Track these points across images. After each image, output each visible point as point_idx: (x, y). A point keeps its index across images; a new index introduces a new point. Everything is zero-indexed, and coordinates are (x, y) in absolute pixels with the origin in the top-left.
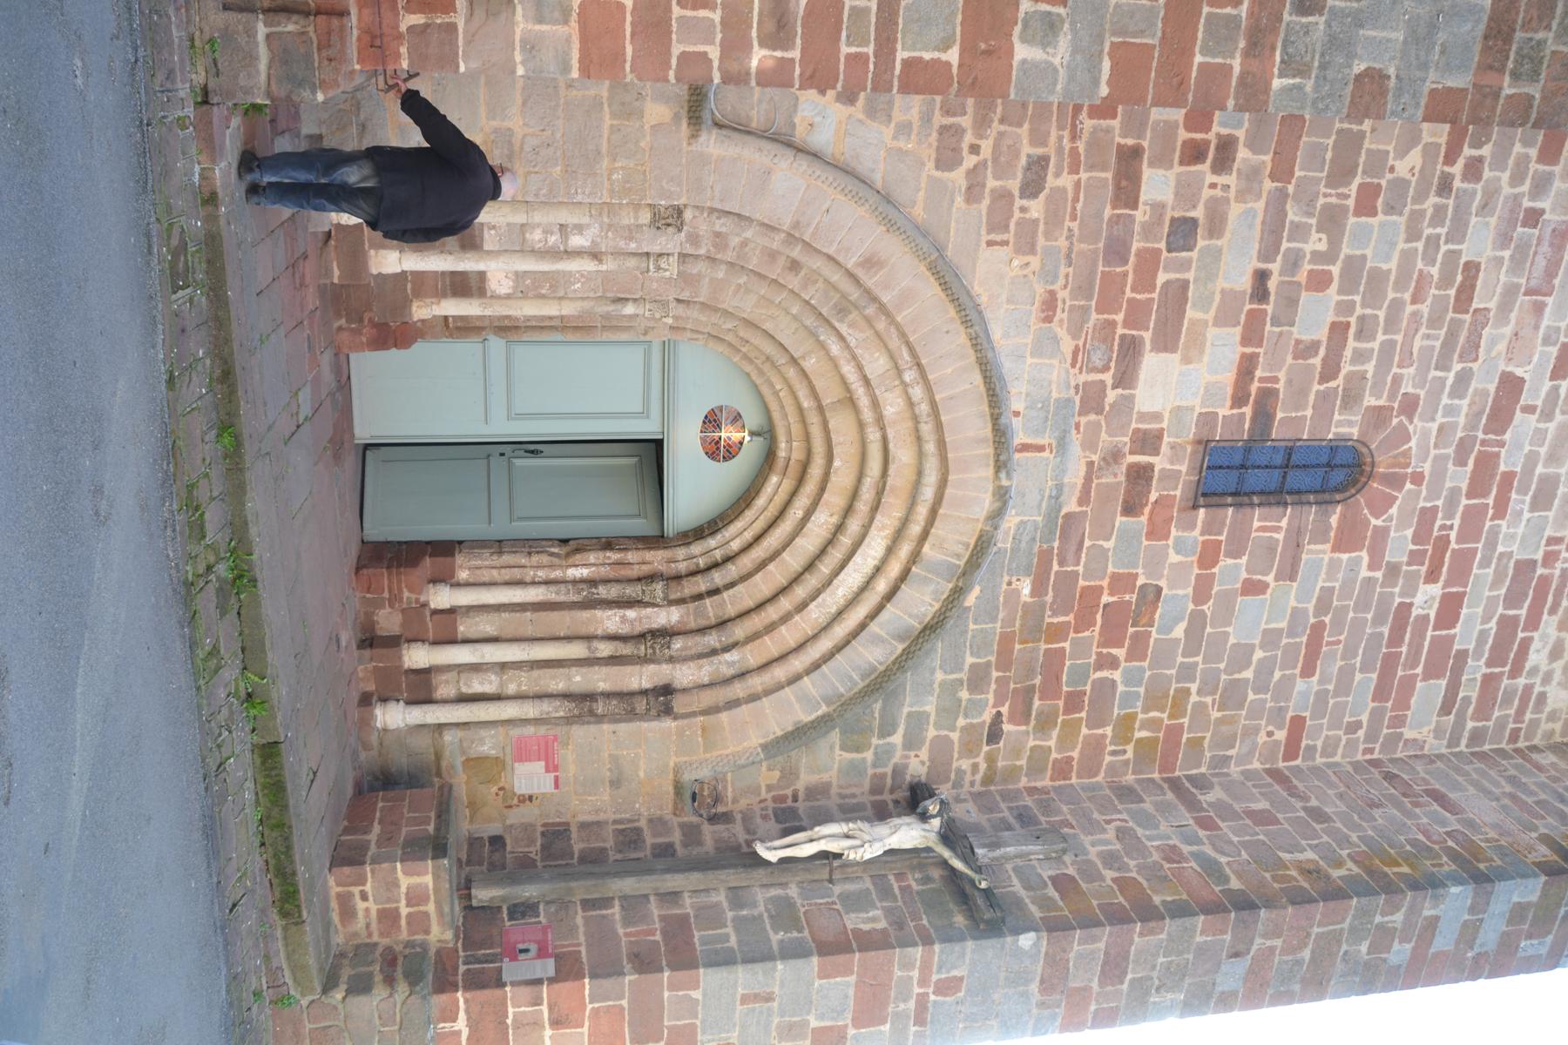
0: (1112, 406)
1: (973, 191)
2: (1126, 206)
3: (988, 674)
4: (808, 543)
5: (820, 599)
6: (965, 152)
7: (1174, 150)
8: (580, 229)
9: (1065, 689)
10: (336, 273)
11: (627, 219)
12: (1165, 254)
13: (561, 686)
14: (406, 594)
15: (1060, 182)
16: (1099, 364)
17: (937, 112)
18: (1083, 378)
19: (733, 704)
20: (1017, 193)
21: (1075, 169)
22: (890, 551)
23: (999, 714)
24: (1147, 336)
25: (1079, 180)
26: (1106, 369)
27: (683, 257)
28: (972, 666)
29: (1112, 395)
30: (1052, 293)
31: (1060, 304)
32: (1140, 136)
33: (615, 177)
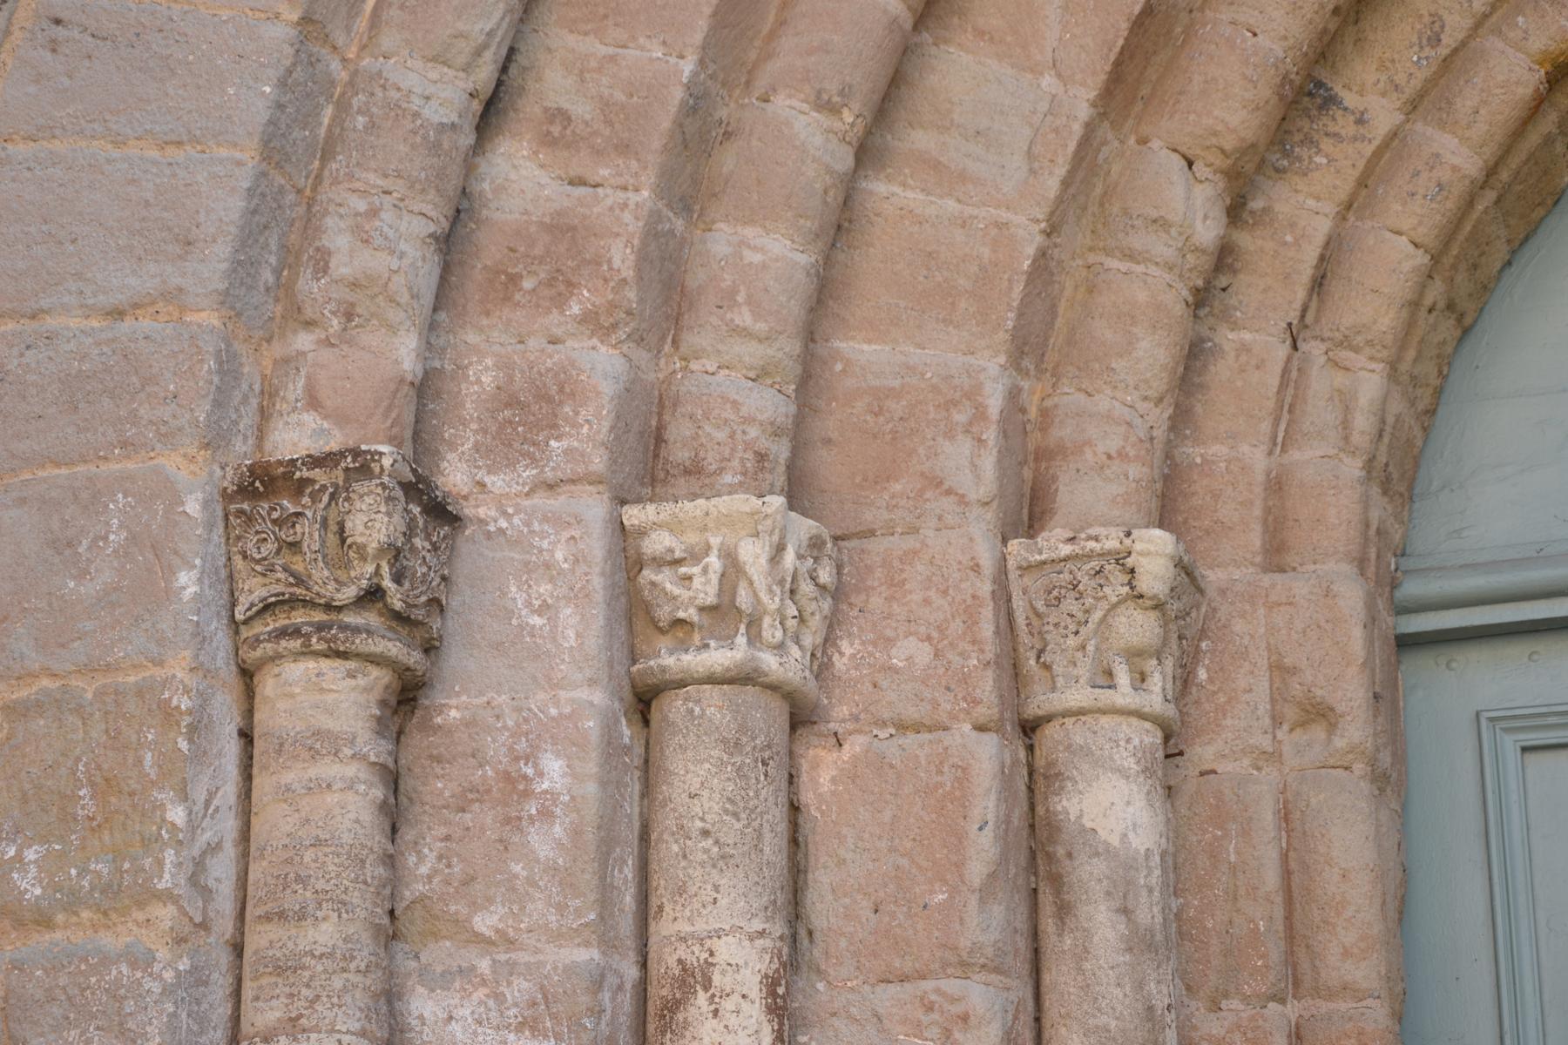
11: (327, 798)
27: (650, 459)
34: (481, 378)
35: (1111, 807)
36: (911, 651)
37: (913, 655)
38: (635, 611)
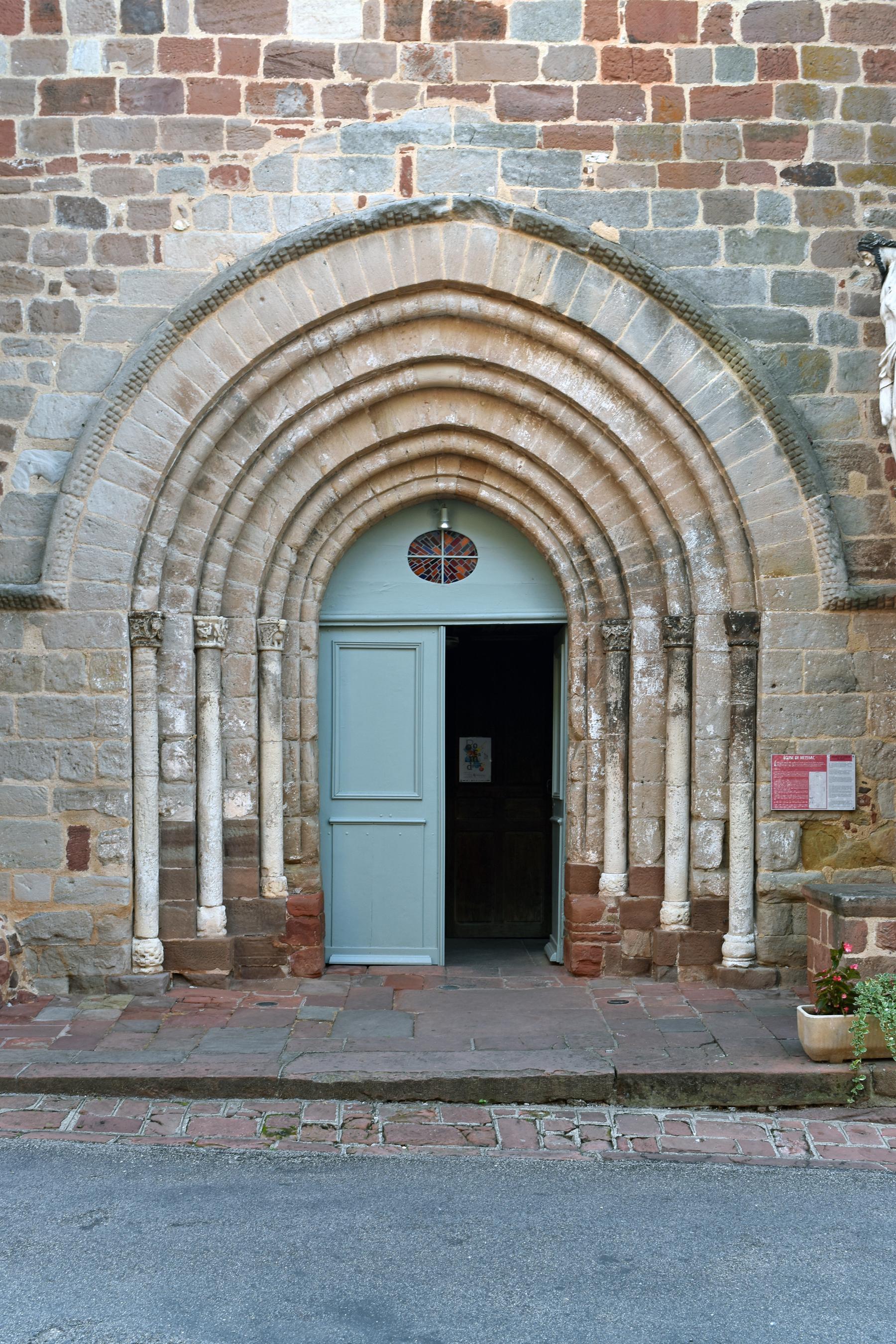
0: (355, 74)
1: (103, 286)
2: (111, 93)
3: (724, 195)
4: (554, 452)
5: (617, 431)
6: (58, 299)
7: (44, 41)
8: (163, 721)
9: (755, 81)
10: (217, 971)
11: (148, 671)
12: (166, 34)
13: (718, 749)
14: (602, 923)
15: (86, 180)
16: (302, 100)
17: (17, 336)
18: (319, 120)
19: (746, 540)
20: (100, 233)
21: (70, 165)
22: (551, 346)
23: (786, 173)
24: (266, 40)
25: (82, 157)
26: (307, 90)
27: (198, 608)
28: (708, 220)
29: (342, 77)
30: (214, 173)
31: (225, 163)
32: (30, 86)
33: (99, 686)
34: (169, 590)
35: (273, 667)
37: (244, 640)
38: (197, 635)
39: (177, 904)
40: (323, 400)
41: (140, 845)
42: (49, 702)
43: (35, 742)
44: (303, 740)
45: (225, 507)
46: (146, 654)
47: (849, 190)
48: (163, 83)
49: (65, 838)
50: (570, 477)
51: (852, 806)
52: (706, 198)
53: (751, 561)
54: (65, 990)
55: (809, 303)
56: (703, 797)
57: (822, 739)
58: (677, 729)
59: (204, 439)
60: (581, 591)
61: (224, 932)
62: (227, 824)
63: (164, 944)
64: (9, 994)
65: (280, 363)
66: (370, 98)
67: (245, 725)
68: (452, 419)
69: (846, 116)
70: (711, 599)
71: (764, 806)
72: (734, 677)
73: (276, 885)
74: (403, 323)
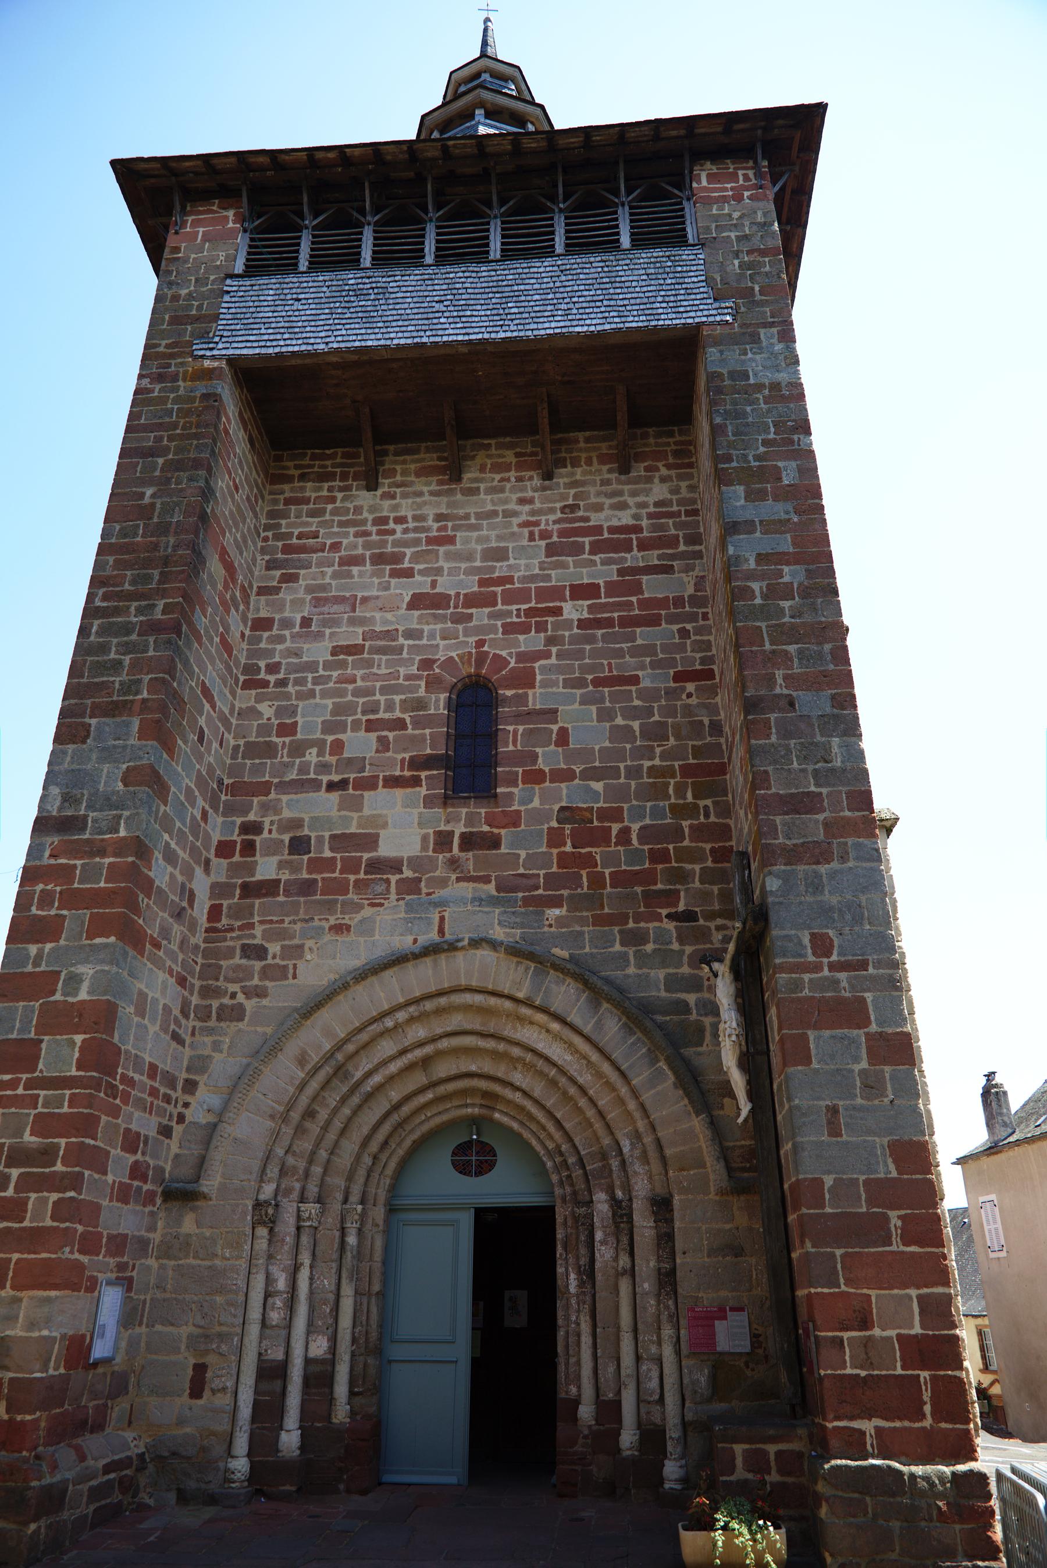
0: (415, 872)
1: (260, 993)
3: (631, 930)
8: (269, 1280)
9: (647, 866)
10: (287, 1488)
11: (262, 1244)
12: (312, 855)
14: (578, 1448)
16: (384, 886)
18: (393, 896)
20: (264, 963)
23: (668, 916)
24: (366, 856)
26: (388, 881)
27: (302, 1199)
28: (622, 944)
29: (408, 873)
30: (331, 928)
32: (235, 885)
35: (352, 1240)
36: (330, 1220)
37: (331, 1220)
38: (299, 1218)
39: (264, 1428)
40: (392, 1058)
41: (242, 1379)
42: (193, 1267)
43: (180, 1297)
44: (370, 1295)
45: (325, 1128)
46: (262, 1232)
47: (708, 924)
48: (307, 880)
49: (190, 1372)
50: (549, 1104)
51: (748, 1349)
52: (620, 932)
53: (664, 1160)
54: (173, 1502)
55: (688, 992)
56: (644, 1341)
57: (724, 1293)
58: (624, 1286)
59: (314, 1085)
60: (561, 1183)
61: (298, 1452)
62: (308, 1361)
63: (251, 1462)
64: (129, 1504)
65: (364, 1037)
66: (423, 884)
67: (327, 1283)
68: (473, 1068)
69: (702, 882)
70: (641, 1187)
71: (685, 1350)
72: (659, 1245)
73: (341, 1413)
74: (439, 1011)
